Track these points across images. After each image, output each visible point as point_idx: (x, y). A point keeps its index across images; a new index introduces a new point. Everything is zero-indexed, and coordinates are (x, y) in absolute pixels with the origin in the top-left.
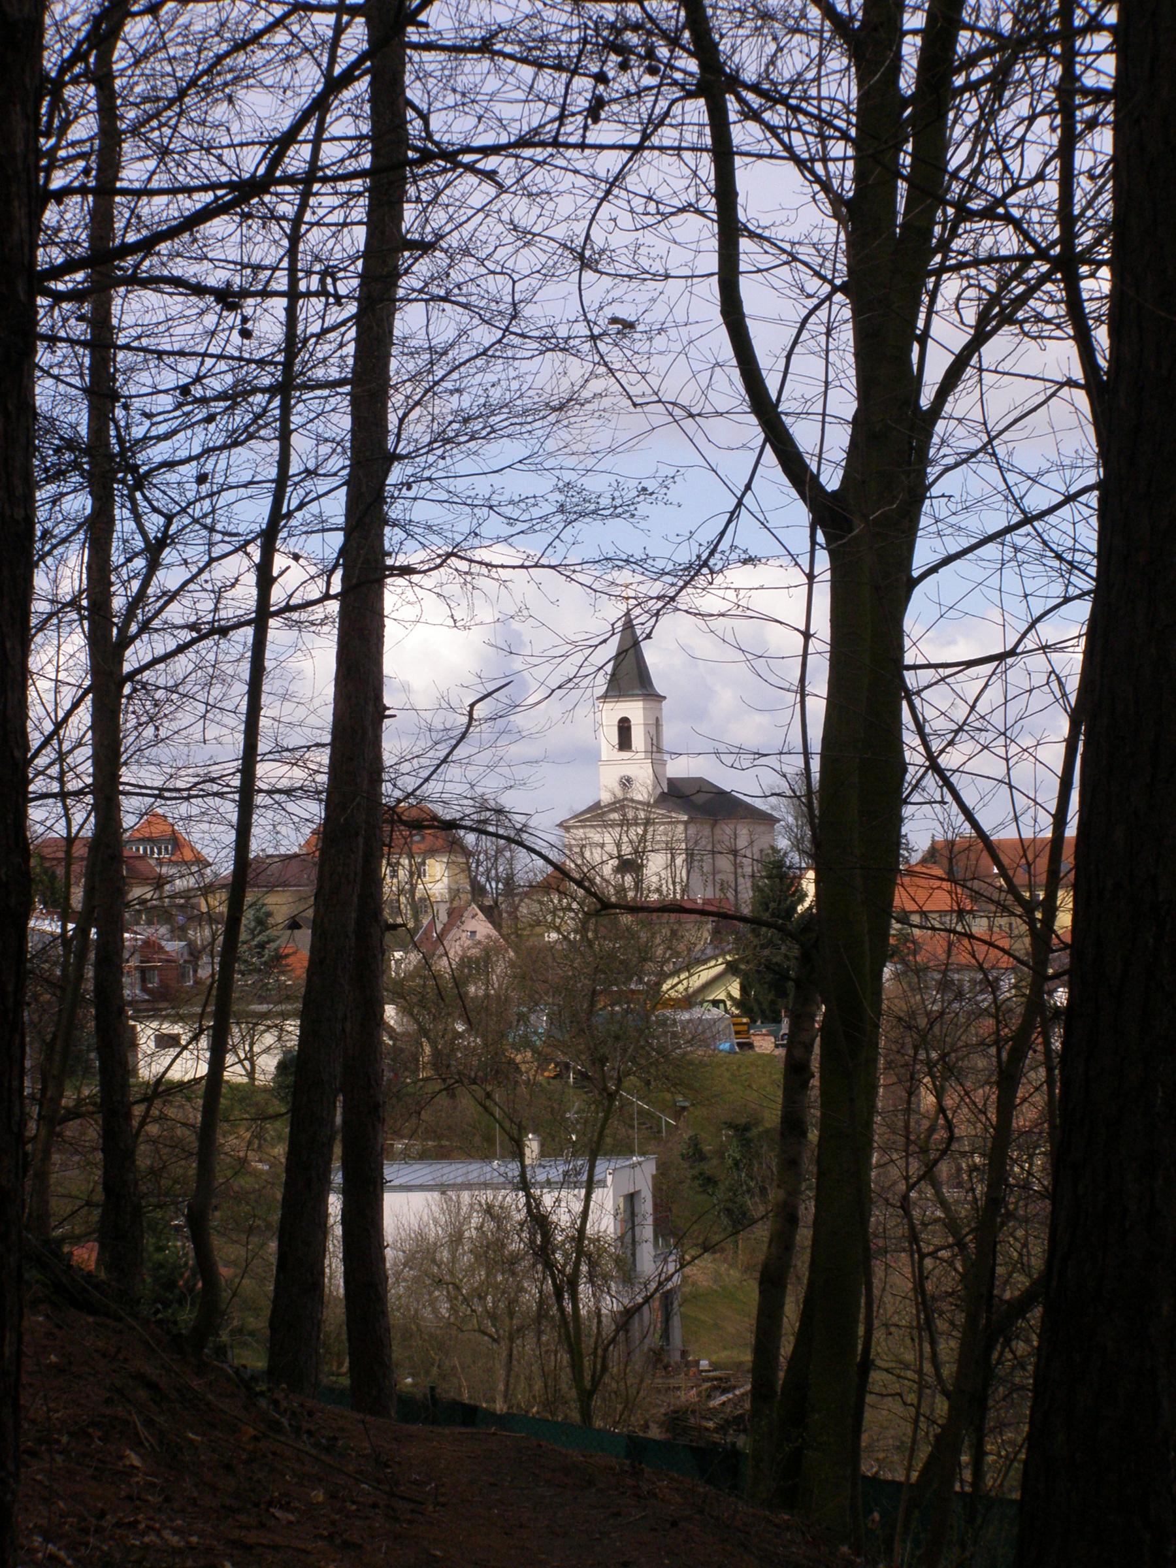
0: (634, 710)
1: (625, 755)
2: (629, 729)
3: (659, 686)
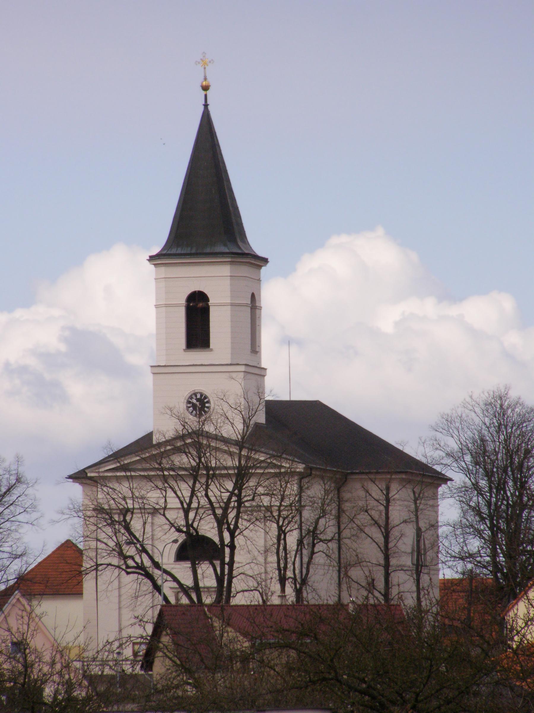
0: (215, 280)
1: (198, 356)
2: (205, 312)
3: (257, 240)
